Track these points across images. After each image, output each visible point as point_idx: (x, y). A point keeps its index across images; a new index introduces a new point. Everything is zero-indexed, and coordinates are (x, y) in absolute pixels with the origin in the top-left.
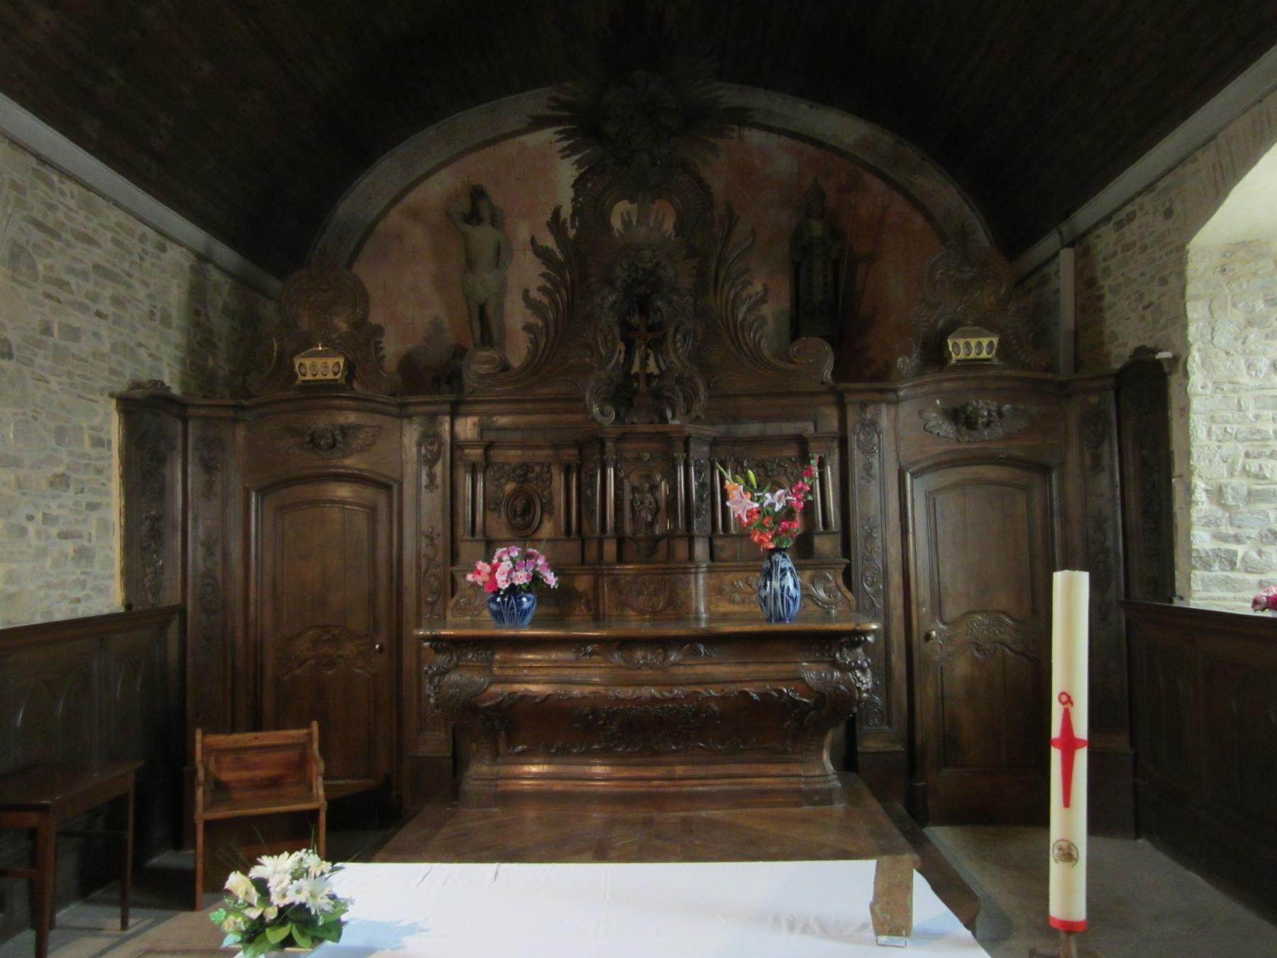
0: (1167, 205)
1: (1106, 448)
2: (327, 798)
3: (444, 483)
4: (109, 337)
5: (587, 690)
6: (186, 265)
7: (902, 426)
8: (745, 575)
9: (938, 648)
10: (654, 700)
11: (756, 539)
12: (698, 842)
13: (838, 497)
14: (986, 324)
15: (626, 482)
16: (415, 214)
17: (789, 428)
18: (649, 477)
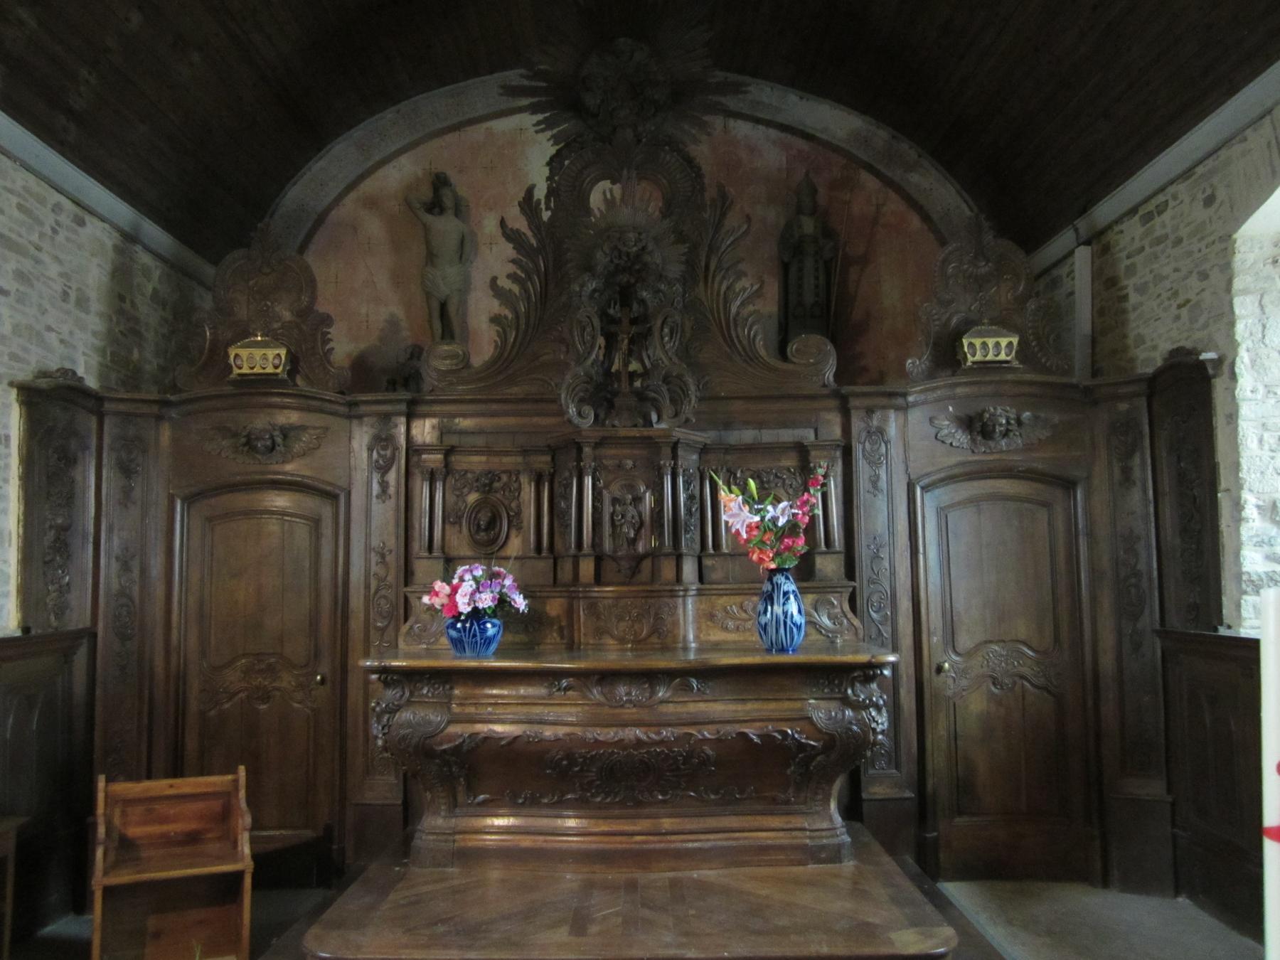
0: (1209, 192)
1: (1137, 460)
2: (255, 857)
3: (398, 493)
4: (11, 317)
5: (562, 731)
6: (109, 244)
7: (914, 436)
8: (738, 599)
9: (950, 681)
10: (639, 743)
11: (755, 557)
12: (692, 912)
13: (841, 513)
14: (1003, 324)
15: (605, 492)
16: (371, 203)
17: (787, 435)
18: (631, 487)
